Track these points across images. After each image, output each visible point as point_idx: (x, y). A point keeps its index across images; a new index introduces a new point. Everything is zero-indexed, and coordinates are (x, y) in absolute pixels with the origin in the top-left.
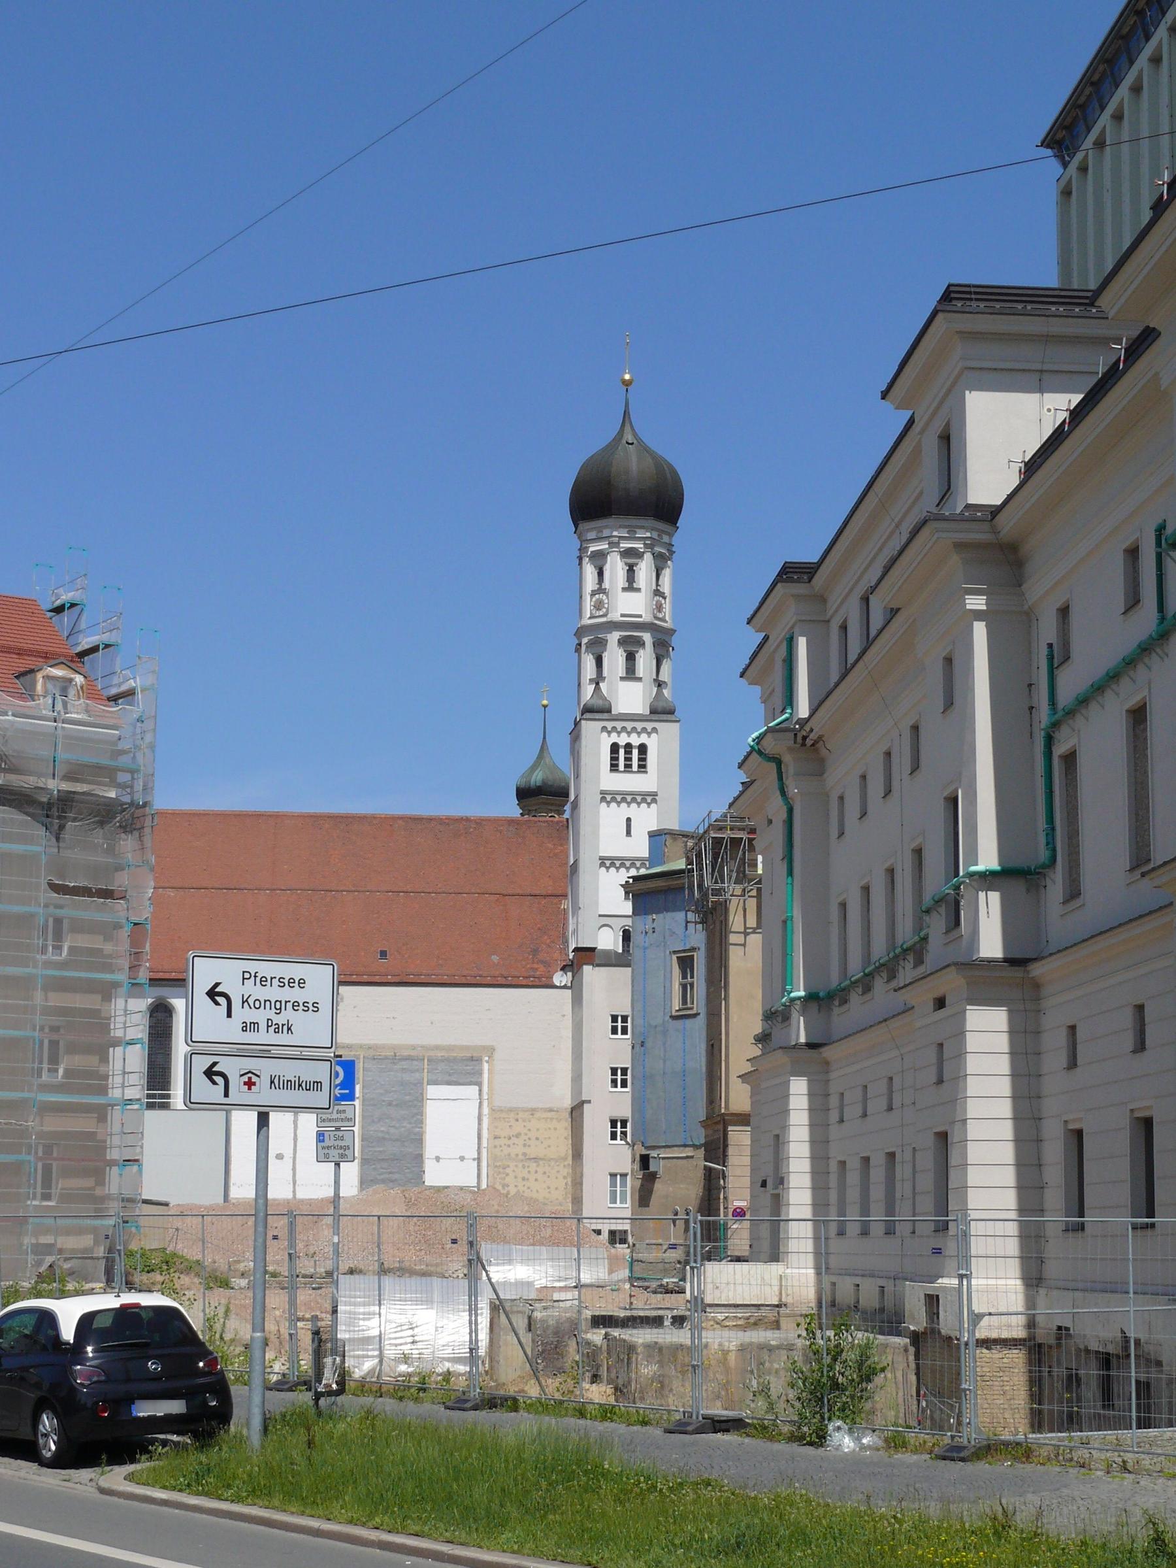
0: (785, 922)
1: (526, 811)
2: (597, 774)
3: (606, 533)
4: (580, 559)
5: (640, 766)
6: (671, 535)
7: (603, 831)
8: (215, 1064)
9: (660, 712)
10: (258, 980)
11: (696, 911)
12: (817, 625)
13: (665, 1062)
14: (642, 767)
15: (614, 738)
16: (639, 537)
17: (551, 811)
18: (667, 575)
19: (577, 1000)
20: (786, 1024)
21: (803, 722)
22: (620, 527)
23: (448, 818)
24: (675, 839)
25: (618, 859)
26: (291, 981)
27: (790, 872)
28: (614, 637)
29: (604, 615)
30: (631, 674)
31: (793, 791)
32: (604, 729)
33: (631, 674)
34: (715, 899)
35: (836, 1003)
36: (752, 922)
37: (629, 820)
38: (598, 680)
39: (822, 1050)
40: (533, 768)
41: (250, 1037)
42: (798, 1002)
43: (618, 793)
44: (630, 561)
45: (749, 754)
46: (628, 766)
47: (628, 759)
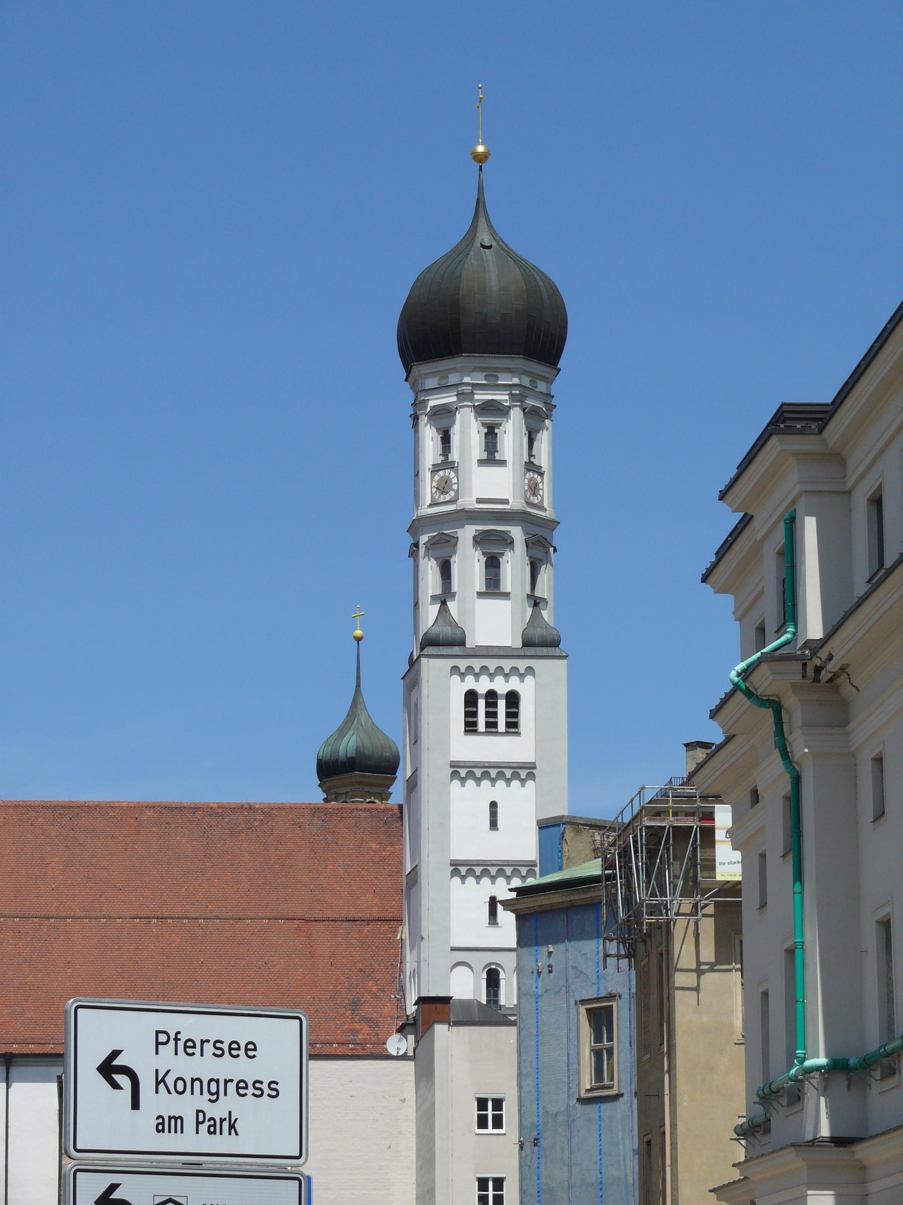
0: (790, 952)
1: (331, 794)
2: (449, 738)
3: (453, 379)
4: (415, 418)
5: (509, 725)
6: (549, 381)
7: (456, 822)
8: (113, 1187)
9: (538, 643)
10: (181, 1045)
11: (622, 941)
12: (833, 498)
13: (570, 1167)
14: (513, 725)
15: (470, 683)
16: (505, 382)
17: (370, 794)
18: (544, 439)
19: (425, 1074)
20: (797, 1107)
21: (815, 647)
22: (476, 369)
23: (222, 807)
24: (578, 832)
25: (478, 863)
26: (234, 1046)
27: (799, 876)
28: (467, 533)
29: (453, 501)
30: (493, 587)
31: (801, 749)
32: (455, 670)
33: (493, 587)
34: (653, 919)
35: (877, 1074)
36: (708, 953)
37: (493, 805)
38: (444, 598)
39: (857, 1148)
40: (342, 731)
41: (169, 1142)
42: (816, 1074)
43: (477, 765)
44: (491, 420)
45: (729, 696)
46: (491, 725)
47: (491, 714)
